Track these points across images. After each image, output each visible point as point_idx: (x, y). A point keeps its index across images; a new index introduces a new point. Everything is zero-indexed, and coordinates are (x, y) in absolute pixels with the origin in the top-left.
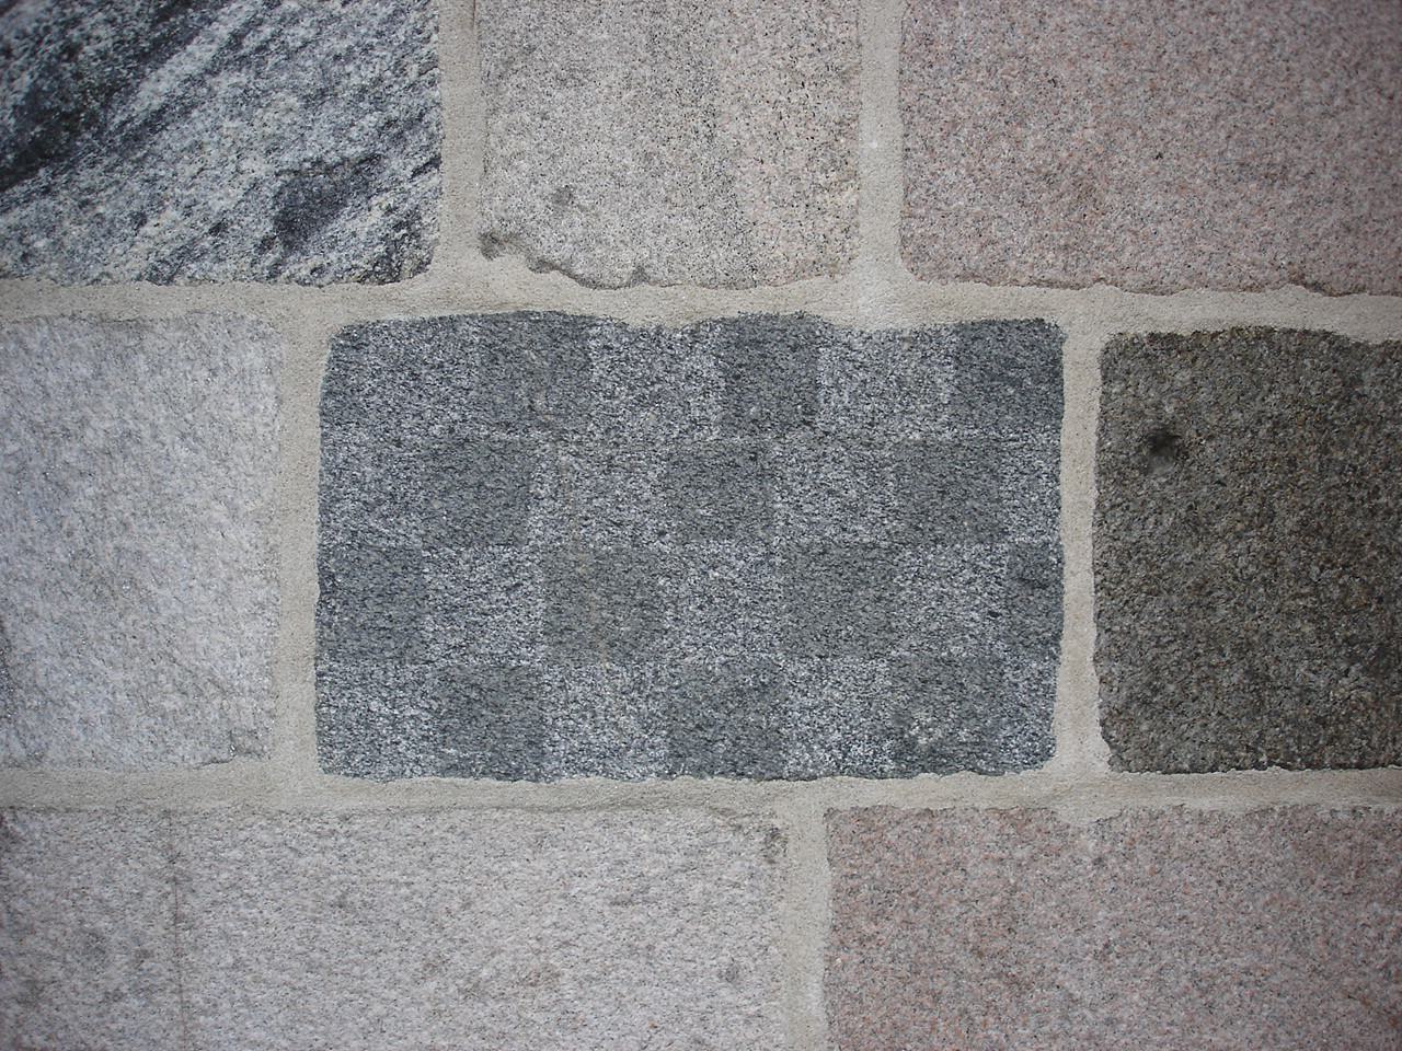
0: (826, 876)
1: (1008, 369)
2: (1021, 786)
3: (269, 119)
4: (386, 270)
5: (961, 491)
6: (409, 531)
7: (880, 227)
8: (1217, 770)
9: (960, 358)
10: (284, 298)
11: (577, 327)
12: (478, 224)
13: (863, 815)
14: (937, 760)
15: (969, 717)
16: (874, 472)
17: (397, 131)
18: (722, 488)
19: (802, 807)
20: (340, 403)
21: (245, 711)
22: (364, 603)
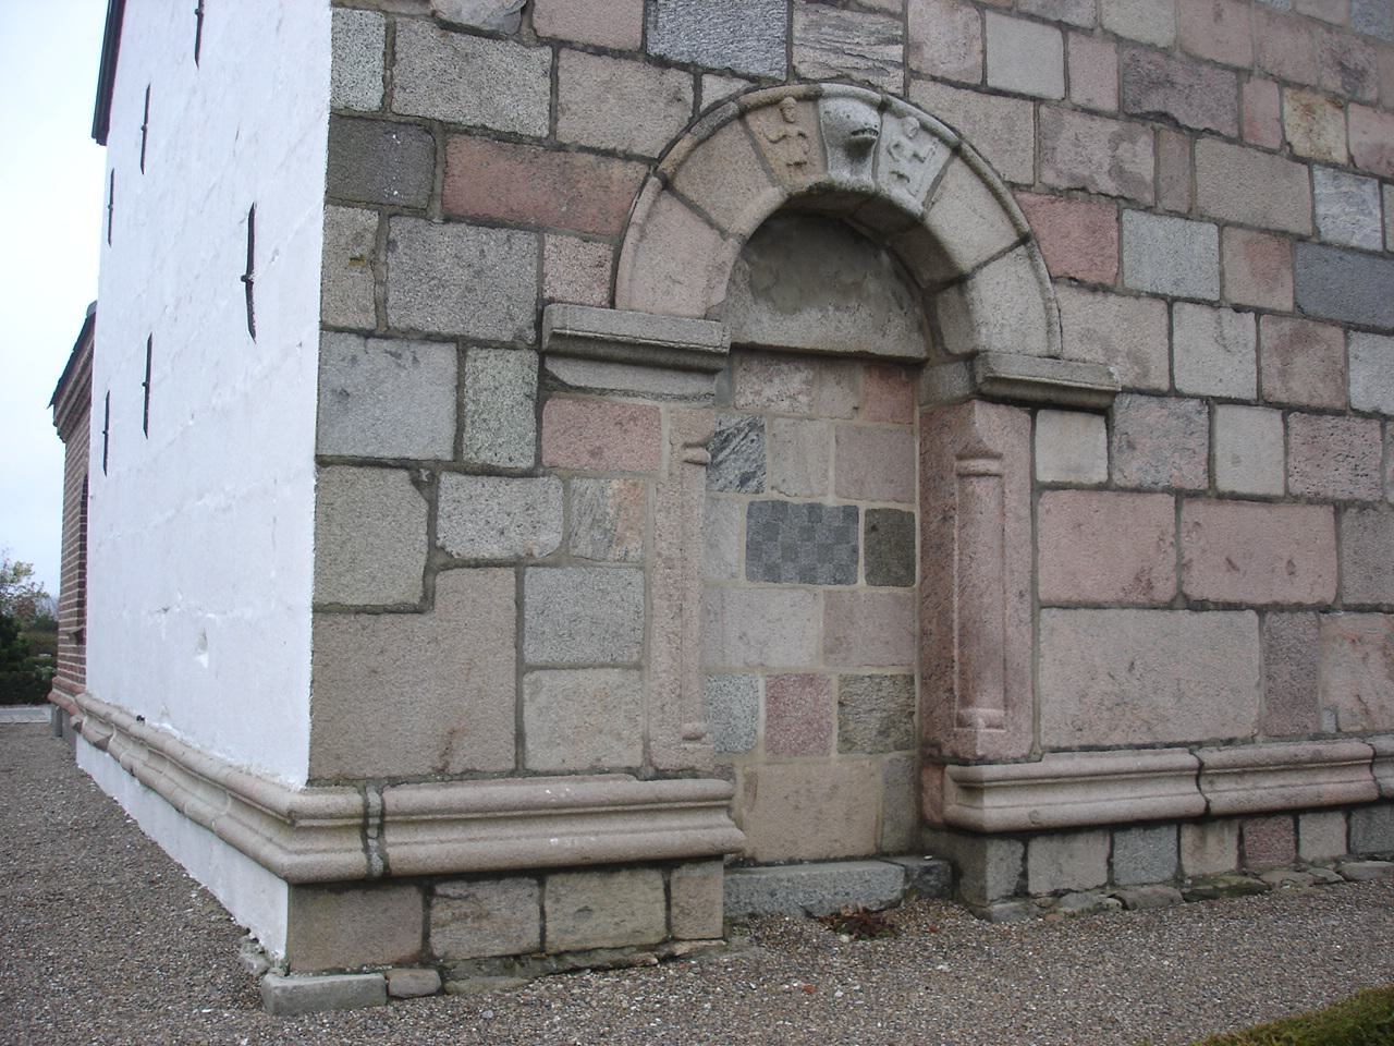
0: (823, 603)
1: (850, 513)
2: (852, 587)
3: (739, 464)
4: (757, 492)
5: (843, 535)
6: (760, 538)
7: (832, 488)
8: (1316, 698)
9: (843, 511)
10: (741, 496)
11: (785, 504)
12: (771, 485)
13: (829, 592)
14: (840, 582)
15: (844, 576)
16: (830, 531)
17: (759, 467)
18: (808, 533)
19: (820, 589)
20: (750, 515)
21: (735, 570)
22: (753, 550)
